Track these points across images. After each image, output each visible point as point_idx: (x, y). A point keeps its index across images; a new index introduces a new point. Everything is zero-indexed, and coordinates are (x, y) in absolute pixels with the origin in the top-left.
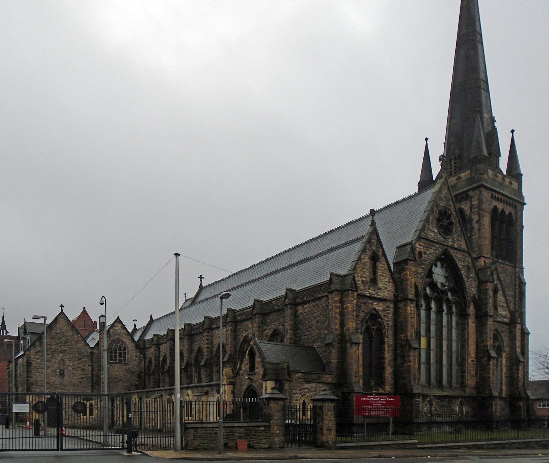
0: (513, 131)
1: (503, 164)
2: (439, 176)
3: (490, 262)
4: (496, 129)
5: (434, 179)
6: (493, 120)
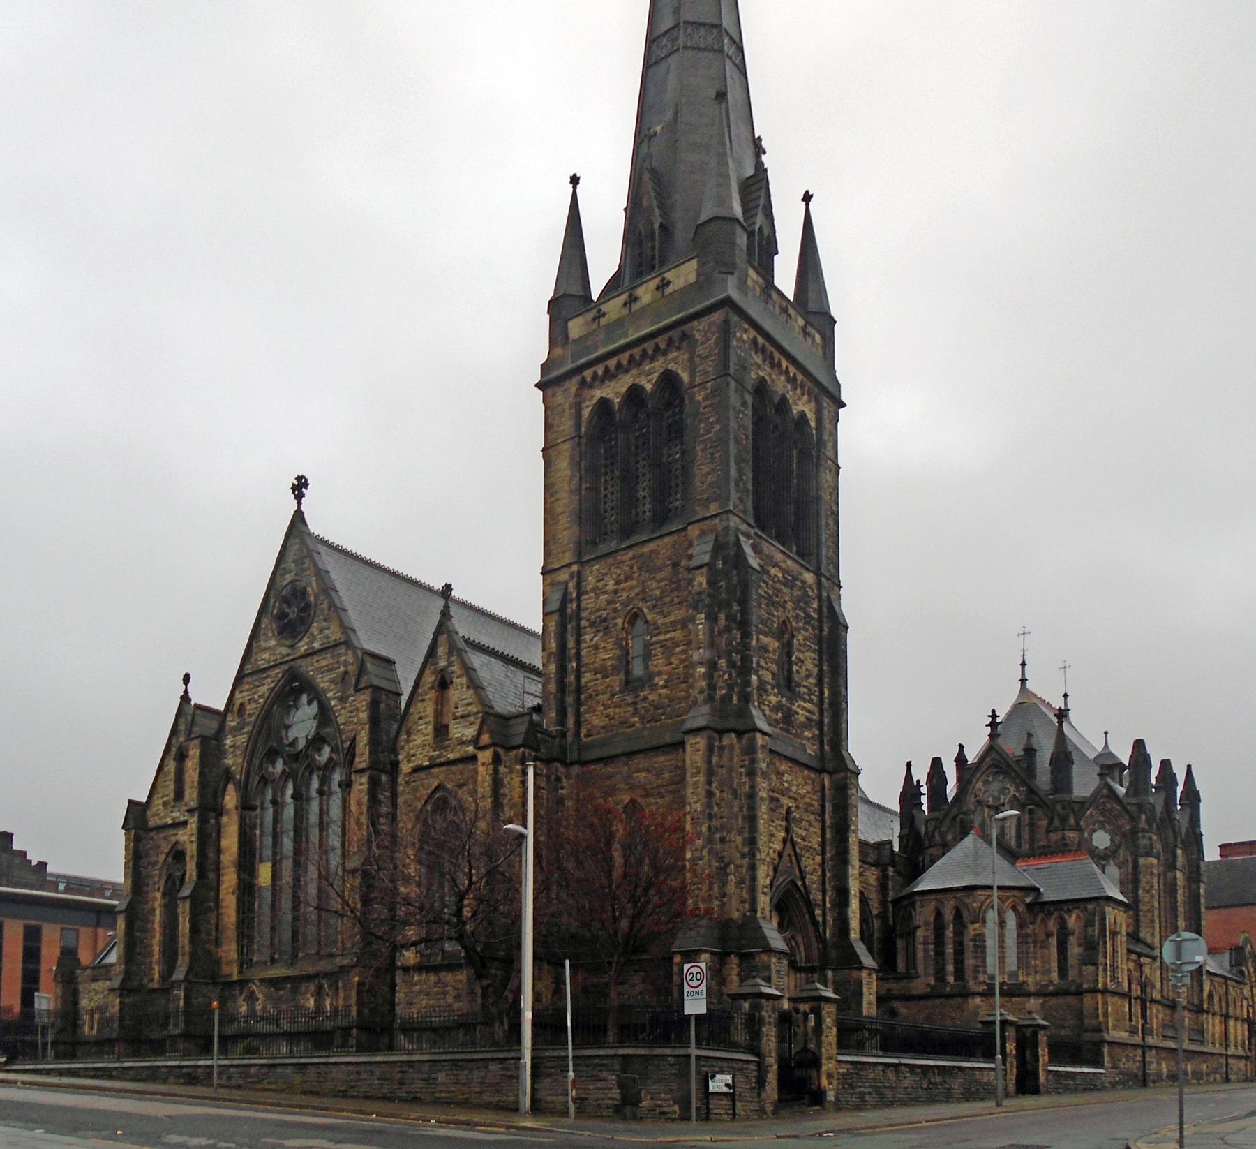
0: (807, 198)
1: (785, 276)
2: (613, 286)
3: (814, 734)
4: (766, 170)
5: (595, 297)
6: (758, 148)
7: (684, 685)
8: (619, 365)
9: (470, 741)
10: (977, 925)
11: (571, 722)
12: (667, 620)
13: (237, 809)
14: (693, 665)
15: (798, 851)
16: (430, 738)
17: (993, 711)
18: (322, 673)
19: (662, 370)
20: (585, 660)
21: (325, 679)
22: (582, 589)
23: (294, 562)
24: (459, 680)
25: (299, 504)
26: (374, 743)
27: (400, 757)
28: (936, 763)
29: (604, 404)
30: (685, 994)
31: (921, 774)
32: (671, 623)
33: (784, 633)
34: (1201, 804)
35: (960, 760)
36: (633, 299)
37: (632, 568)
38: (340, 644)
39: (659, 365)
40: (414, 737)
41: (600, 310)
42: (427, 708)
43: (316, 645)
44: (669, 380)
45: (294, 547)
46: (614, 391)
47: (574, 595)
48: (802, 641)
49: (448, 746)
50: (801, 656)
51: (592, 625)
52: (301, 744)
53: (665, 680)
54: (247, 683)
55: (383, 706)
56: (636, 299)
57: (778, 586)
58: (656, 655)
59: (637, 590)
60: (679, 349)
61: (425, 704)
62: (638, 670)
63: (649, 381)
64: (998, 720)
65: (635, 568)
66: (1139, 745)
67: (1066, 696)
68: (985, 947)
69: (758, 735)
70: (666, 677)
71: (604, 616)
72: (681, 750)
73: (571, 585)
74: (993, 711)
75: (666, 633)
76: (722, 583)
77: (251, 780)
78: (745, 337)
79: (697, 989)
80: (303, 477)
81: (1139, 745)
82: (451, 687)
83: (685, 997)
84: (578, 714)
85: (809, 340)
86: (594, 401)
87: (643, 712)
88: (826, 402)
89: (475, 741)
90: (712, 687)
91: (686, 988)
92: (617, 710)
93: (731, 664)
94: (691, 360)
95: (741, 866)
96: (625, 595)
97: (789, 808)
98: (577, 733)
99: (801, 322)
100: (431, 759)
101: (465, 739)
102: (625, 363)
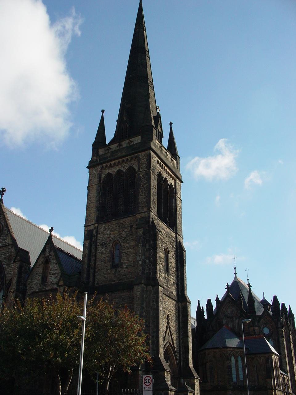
2: (112, 142)
4: (160, 115)
5: (107, 143)
7: (133, 268)
9: (56, 283)
10: (228, 362)
11: (91, 279)
12: (128, 245)
14: (138, 261)
15: (171, 331)
16: (40, 282)
17: (227, 284)
18: (2, 255)
19: (129, 166)
21: (2, 257)
22: (98, 233)
26: (18, 282)
27: (28, 288)
28: (209, 301)
29: (109, 175)
30: (144, 388)
31: (204, 305)
32: (129, 246)
33: (167, 252)
34: (295, 319)
35: (217, 300)
36: (120, 145)
37: (116, 227)
38: (10, 245)
39: (127, 165)
40: (33, 280)
42: (40, 270)
44: (131, 169)
46: (113, 171)
47: (95, 234)
48: (171, 256)
49: (47, 285)
50: (171, 260)
51: (101, 245)
53: (127, 266)
55: (23, 269)
56: (121, 145)
57: (164, 236)
58: (123, 257)
59: (118, 234)
60: (134, 161)
61: (39, 269)
62: (117, 261)
63: (124, 169)
64: (229, 286)
66: (275, 298)
67: (248, 280)
68: (232, 371)
69: (159, 287)
70: (127, 265)
72: (132, 291)
73: (95, 231)
74: (227, 284)
75: (127, 249)
76: (147, 234)
78: (155, 159)
79: (149, 386)
80: (4, 188)
81: (275, 298)
82: (50, 263)
83: (144, 390)
85: (173, 162)
86: (106, 173)
87: (118, 277)
88: (177, 181)
89: (57, 284)
90: (143, 269)
91: (144, 386)
92: (108, 275)
93: (150, 261)
94: (139, 164)
95: (153, 336)
97: (168, 315)
98: (94, 283)
99: (171, 157)
100: (39, 289)
101: (53, 282)
102: (113, 164)
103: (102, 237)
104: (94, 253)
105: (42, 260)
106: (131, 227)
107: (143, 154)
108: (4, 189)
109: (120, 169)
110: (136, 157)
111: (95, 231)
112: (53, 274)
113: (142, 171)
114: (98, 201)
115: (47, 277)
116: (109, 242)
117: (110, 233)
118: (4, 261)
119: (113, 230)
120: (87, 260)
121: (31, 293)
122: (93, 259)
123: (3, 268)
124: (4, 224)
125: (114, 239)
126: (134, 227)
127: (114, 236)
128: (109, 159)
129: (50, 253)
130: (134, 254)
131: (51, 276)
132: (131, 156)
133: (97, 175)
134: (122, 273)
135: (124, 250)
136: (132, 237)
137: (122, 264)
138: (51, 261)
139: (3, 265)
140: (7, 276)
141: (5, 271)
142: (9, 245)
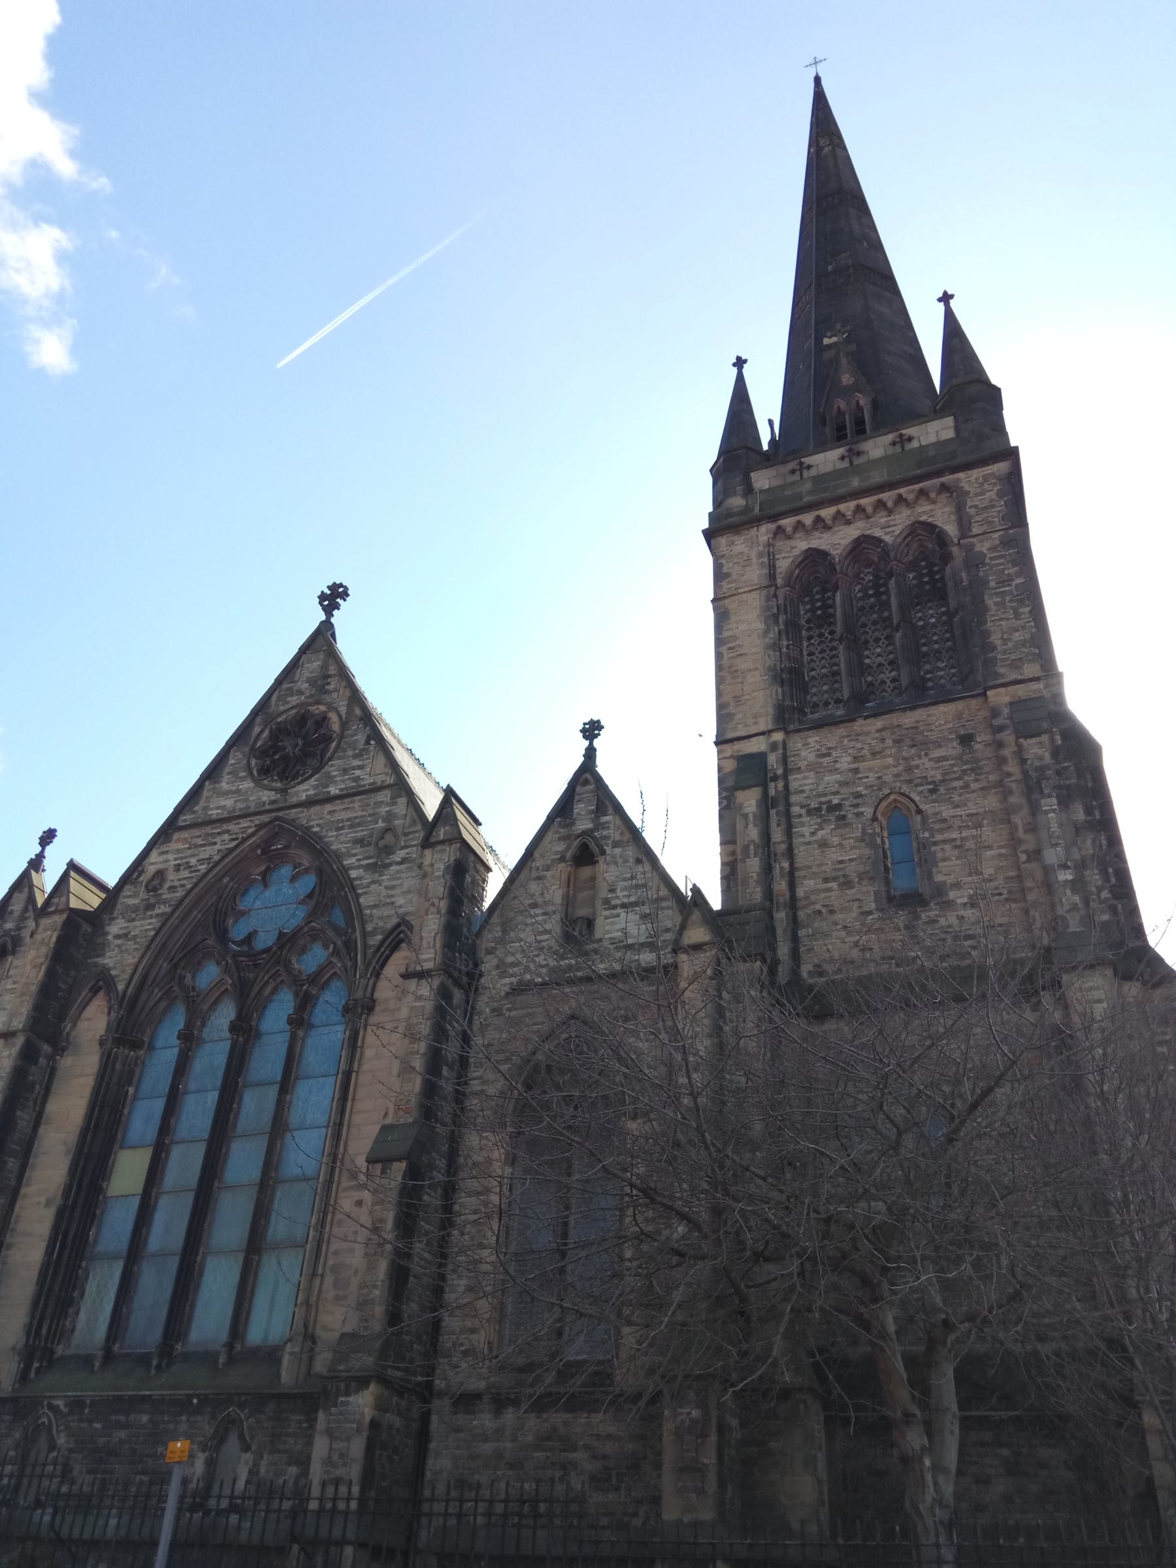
8: (839, 515)
12: (959, 812)
13: (102, 1043)
18: (338, 829)
20: (800, 861)
21: (342, 839)
23: (308, 680)
24: (617, 851)
25: (43, 849)
29: (815, 557)
32: (969, 815)
37: (883, 740)
41: (801, 464)
43: (333, 790)
45: (313, 666)
47: (780, 772)
51: (810, 812)
52: (265, 940)
53: (970, 897)
54: (178, 840)
58: (944, 860)
60: (933, 502)
65: (889, 742)
71: (835, 801)
77: (144, 996)
80: (341, 585)
84: (795, 939)
86: (796, 552)
94: (960, 509)
96: (872, 778)
100: (552, 970)
103: (810, 781)
104: (782, 842)
105: (560, 847)
106: (966, 740)
107: (974, 476)
108: (341, 590)
109: (868, 532)
110: (944, 488)
111: (773, 759)
112: (624, 906)
113: (985, 533)
114: (775, 646)
115: (590, 923)
116: (856, 801)
117: (853, 766)
118: (355, 855)
119: (865, 752)
120: (757, 869)
121: (507, 989)
122: (782, 869)
123: (351, 881)
124: (350, 710)
125: (880, 789)
126: (979, 740)
127: (879, 778)
128: (807, 499)
129: (597, 817)
130: (1000, 847)
131: (615, 912)
132: (917, 487)
133: (753, 556)
134: (949, 926)
135: (941, 831)
136: (976, 780)
137: (940, 890)
138: (608, 850)
139: (347, 872)
140: (371, 915)
141: (358, 896)
142: (376, 789)
